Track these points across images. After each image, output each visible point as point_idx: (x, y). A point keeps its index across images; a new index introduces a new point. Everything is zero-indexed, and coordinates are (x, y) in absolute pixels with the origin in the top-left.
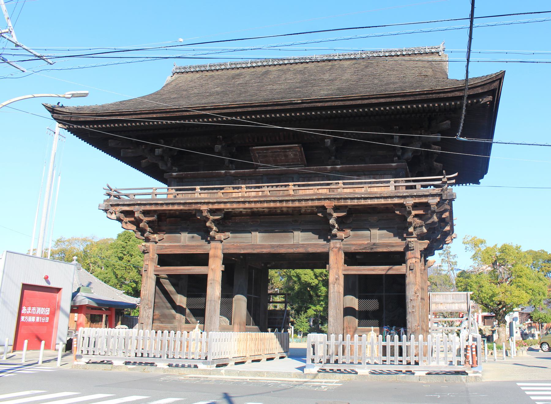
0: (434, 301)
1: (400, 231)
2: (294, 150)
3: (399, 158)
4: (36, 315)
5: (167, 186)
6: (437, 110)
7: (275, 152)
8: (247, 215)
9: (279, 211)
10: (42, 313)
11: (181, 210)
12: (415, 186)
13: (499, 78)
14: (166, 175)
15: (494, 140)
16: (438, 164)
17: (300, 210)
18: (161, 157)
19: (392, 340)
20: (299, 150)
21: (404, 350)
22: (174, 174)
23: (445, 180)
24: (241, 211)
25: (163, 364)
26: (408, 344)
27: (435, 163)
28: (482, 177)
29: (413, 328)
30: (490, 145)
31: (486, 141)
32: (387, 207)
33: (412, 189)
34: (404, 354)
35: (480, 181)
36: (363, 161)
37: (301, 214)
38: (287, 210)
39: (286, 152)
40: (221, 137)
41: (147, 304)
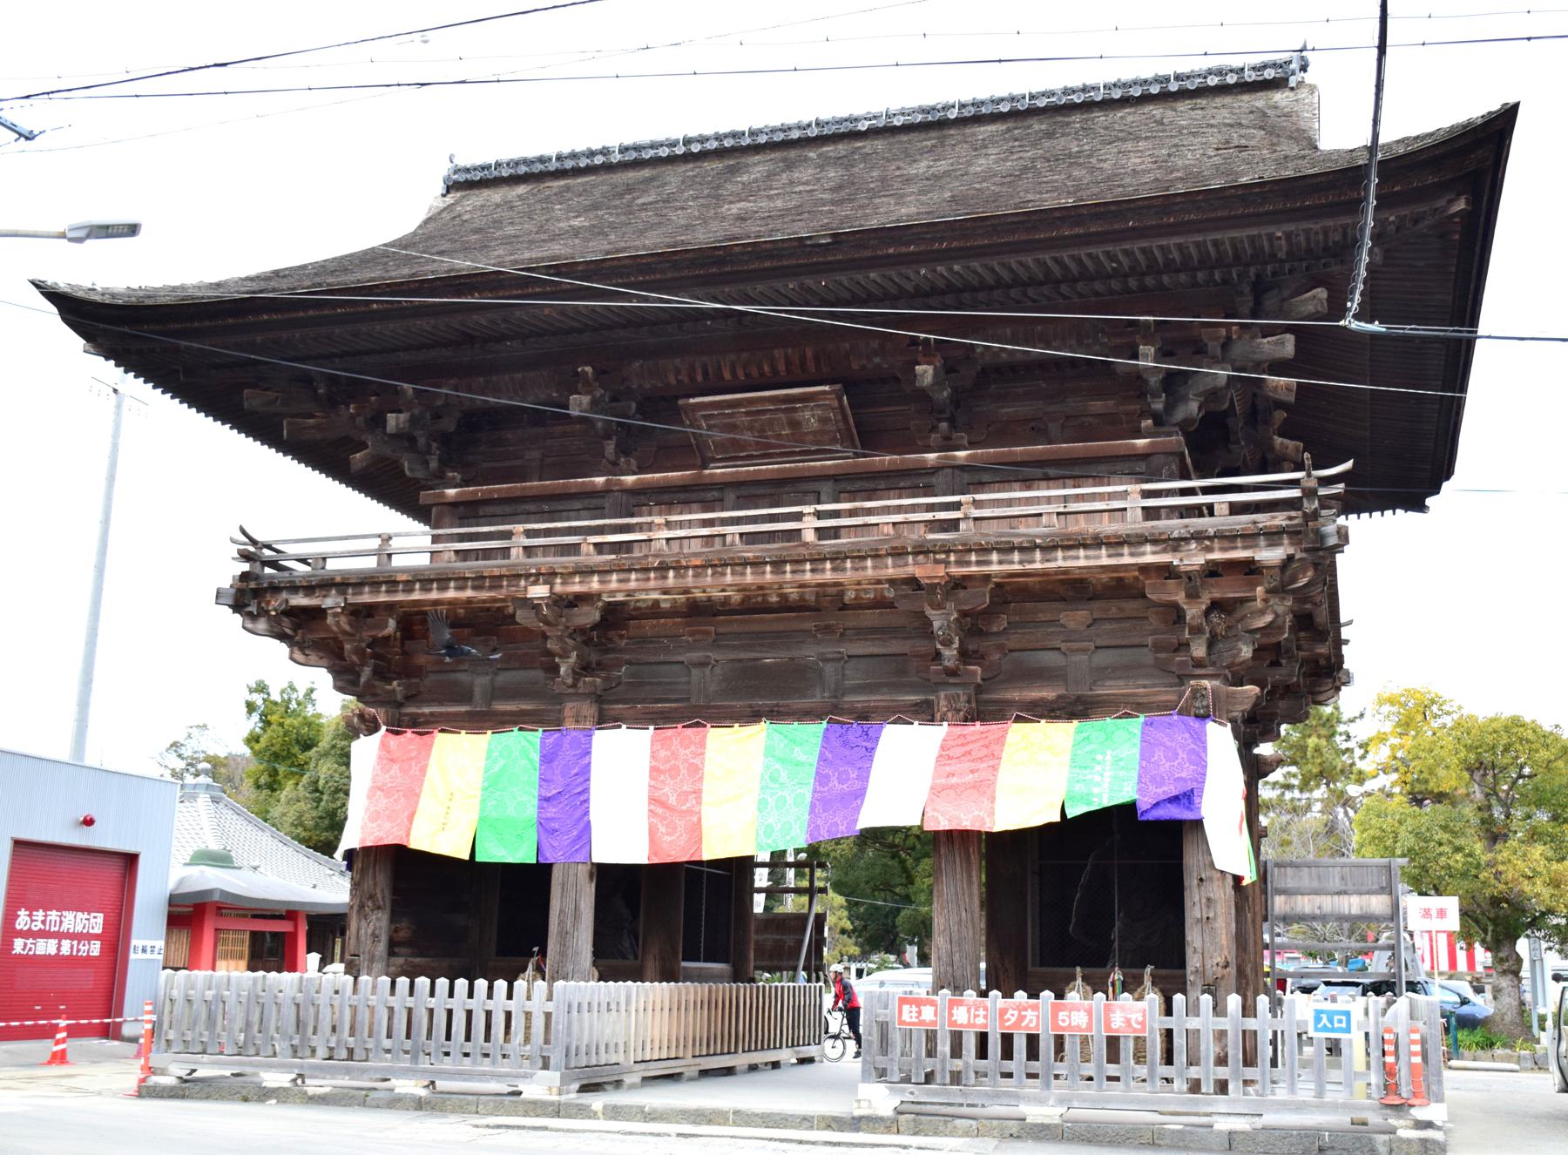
0: (1281, 885)
1: (1162, 655)
2: (819, 402)
3: (1159, 420)
4: (60, 936)
5: (427, 528)
6: (1282, 255)
7: (759, 412)
8: (673, 613)
9: (774, 599)
10: (79, 929)
11: (469, 601)
12: (1210, 507)
13: (1497, 130)
14: (425, 497)
15: (1481, 330)
16: (1287, 441)
17: (841, 594)
18: (405, 439)
19: (1219, 1009)
20: (836, 404)
21: (1179, 1042)
22: (451, 492)
23: (1312, 483)
24: (657, 602)
25: (413, 1082)
26: (1193, 1023)
27: (1278, 440)
28: (1436, 490)
29: (1209, 973)
30: (1469, 346)
31: (1449, 331)
32: (1120, 579)
33: (1201, 515)
34: (1180, 1056)
35: (1429, 501)
36: (1038, 432)
37: (845, 607)
38: (802, 595)
39: (795, 410)
40: (588, 369)
41: (371, 897)
